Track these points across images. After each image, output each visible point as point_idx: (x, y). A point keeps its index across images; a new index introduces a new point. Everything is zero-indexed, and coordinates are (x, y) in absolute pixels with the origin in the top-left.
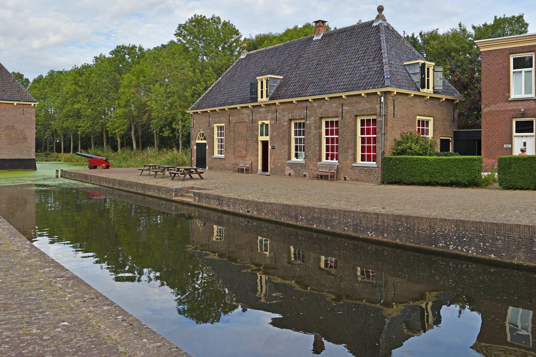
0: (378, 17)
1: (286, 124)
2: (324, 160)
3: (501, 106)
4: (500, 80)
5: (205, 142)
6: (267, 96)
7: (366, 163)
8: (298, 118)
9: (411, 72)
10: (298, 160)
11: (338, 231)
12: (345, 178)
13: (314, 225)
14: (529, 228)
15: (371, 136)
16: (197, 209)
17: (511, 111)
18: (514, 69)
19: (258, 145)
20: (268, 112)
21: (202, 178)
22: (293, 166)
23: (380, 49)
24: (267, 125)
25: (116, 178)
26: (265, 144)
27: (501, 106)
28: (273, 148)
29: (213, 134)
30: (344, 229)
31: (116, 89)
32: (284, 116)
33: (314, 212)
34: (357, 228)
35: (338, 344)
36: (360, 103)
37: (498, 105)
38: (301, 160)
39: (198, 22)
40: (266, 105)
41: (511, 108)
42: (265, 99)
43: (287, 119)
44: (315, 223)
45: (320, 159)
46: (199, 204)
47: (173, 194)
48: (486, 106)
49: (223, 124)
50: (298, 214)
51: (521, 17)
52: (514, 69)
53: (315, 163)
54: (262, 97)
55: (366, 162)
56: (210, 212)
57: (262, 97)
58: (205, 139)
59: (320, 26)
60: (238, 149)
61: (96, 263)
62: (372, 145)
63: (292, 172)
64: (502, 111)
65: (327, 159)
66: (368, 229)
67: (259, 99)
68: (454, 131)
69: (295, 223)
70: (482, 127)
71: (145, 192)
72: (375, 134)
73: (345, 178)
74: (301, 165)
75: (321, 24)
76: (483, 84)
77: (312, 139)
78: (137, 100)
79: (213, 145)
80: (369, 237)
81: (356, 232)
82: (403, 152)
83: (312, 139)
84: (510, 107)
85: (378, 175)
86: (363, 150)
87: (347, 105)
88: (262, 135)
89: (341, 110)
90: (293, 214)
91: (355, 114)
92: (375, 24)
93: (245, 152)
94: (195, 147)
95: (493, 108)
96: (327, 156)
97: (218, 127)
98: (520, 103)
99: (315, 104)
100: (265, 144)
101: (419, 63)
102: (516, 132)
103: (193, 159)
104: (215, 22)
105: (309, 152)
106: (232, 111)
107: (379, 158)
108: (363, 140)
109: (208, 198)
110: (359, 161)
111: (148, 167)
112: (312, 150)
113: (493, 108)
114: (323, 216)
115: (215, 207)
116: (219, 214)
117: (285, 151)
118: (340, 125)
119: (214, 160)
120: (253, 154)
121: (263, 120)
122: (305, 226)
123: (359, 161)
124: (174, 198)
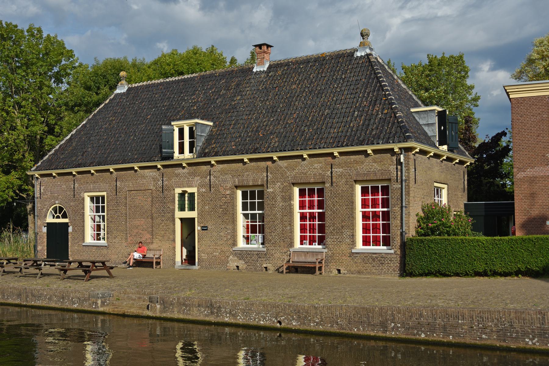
0: (362, 45)
1: (228, 192)
2: (297, 245)
4: (538, 136)
5: (66, 220)
6: (191, 151)
7: (372, 248)
8: (251, 184)
9: (421, 122)
10: (250, 246)
11: (468, 340)
12: (339, 271)
13: (420, 335)
15: (257, 212)
16: (158, 322)
18: (195, 265)
19: (174, 224)
20: (193, 174)
21: (111, 276)
22: (242, 254)
23: (382, 87)
24: (192, 195)
26: (188, 223)
28: (204, 228)
29: (83, 208)
30: (481, 338)
32: (225, 181)
33: (421, 315)
34: (505, 335)
36: (362, 163)
37: (536, 169)
38: (256, 246)
40: (189, 165)
43: (229, 185)
44: (422, 332)
45: (291, 244)
46: (164, 315)
47: (99, 302)
48: (520, 169)
49: (104, 194)
50: (387, 320)
51: (461, 57)
52: (362, 208)
53: (285, 250)
54: (181, 151)
55: (371, 247)
56: (191, 326)
57: (181, 151)
58: (65, 216)
59: (265, 52)
60: (136, 231)
62: (257, 201)
63: (241, 264)
64: (542, 177)
65: (302, 243)
66: (525, 334)
67: (176, 155)
68: (465, 204)
69: (380, 334)
70: (326, 219)
71: (27, 301)
73: (339, 271)
74: (259, 254)
75: (265, 48)
76: (516, 278)
77: (279, 215)
78: (411, 245)
79: (83, 226)
80: (528, 347)
81: (504, 341)
82: (433, 231)
83: (279, 215)
85: (396, 264)
86: (366, 229)
87: (340, 165)
88: (182, 209)
89: (329, 173)
90: (377, 321)
91: (355, 178)
92: (359, 54)
93: (148, 236)
94: (45, 230)
95: (529, 172)
96: (303, 239)
97: (92, 198)
99: (283, 164)
100: (188, 223)
101: (434, 110)
103: (39, 248)
104: (32, 35)
105: (273, 235)
106: (46, 179)
107: (397, 241)
108: (303, 217)
109: (184, 304)
110: (359, 246)
112: (279, 230)
113: (529, 172)
114: (439, 321)
115: (201, 318)
116: (302, 336)
117: (228, 234)
118: (327, 193)
119: (87, 249)
120: (166, 238)
121: (184, 187)
122: (404, 336)
123: (359, 246)
124: (101, 309)
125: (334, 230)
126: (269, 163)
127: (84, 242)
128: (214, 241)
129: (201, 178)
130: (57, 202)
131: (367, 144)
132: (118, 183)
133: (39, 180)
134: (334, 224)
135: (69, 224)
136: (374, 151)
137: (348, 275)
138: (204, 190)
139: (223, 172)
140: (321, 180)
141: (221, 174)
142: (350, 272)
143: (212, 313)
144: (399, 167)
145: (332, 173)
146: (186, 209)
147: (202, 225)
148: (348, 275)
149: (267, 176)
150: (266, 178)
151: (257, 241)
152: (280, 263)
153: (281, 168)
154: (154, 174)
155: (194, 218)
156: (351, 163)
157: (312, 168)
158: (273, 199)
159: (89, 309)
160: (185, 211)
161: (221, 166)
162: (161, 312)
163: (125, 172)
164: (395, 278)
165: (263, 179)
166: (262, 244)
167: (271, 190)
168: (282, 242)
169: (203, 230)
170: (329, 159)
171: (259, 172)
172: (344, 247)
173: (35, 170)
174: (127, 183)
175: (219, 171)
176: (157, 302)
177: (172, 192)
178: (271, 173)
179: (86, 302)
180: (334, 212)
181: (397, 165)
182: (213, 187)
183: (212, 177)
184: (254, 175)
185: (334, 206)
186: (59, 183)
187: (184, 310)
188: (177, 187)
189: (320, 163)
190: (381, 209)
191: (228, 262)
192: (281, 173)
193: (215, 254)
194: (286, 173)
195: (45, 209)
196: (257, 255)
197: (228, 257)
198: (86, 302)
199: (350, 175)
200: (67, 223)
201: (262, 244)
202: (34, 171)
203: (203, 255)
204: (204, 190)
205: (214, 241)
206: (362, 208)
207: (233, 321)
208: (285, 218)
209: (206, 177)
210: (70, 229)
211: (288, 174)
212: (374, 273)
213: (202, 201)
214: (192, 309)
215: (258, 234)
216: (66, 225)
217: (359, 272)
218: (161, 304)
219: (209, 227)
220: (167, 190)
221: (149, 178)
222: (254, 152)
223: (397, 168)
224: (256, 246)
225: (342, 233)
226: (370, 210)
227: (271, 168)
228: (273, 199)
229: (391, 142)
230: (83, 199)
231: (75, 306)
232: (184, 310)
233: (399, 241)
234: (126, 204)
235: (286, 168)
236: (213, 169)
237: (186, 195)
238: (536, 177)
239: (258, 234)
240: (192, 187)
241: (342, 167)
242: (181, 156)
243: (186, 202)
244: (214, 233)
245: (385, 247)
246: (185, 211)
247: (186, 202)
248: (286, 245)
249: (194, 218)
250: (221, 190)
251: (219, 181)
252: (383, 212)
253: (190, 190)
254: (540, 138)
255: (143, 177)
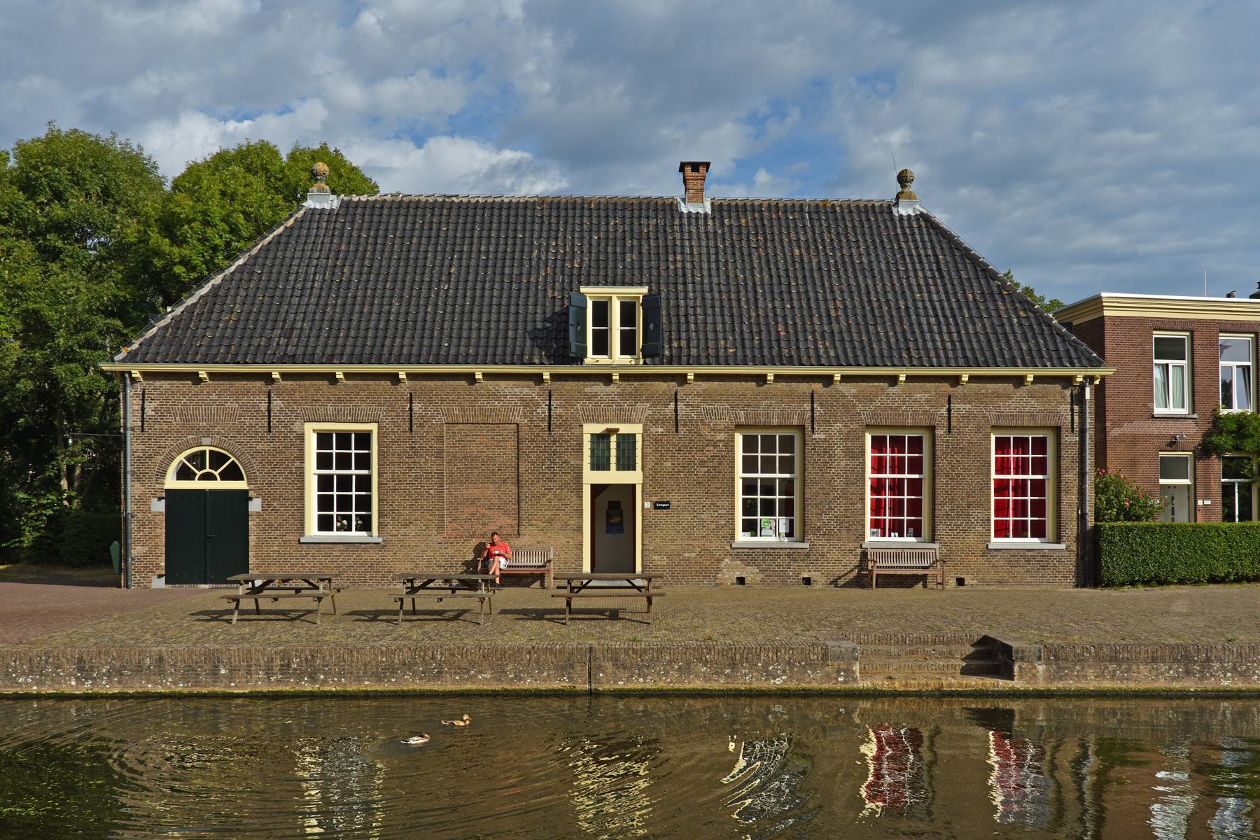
3: (1140, 427)
5: (240, 485)
14: (780, 356)
17: (1157, 436)
20: (636, 398)
25: (1092, 590)
27: (1140, 427)
31: (269, 505)
35: (181, 582)
36: (1009, 397)
39: (985, 640)
40: (624, 377)
41: (1156, 432)
42: (617, 356)
46: (1054, 686)
48: (1115, 424)
51: (619, 503)
52: (318, 468)
54: (602, 346)
55: (335, 533)
56: (1132, 704)
58: (232, 473)
61: (479, 549)
63: (750, 574)
64: (1143, 436)
72: (695, 380)
73: (960, 582)
84: (1154, 429)
85: (1070, 566)
87: (965, 399)
89: (944, 411)
91: (994, 422)
94: (160, 507)
95: (1127, 429)
98: (1171, 423)
99: (851, 389)
102: (996, 536)
107: (1071, 530)
111: (590, 584)
113: (1127, 429)
119: (314, 550)
120: (557, 525)
123: (312, 530)
125: (952, 510)
126: (817, 386)
127: (302, 534)
128: (684, 529)
129: (654, 405)
130: (206, 441)
131: (688, 364)
132: (417, 407)
133: (139, 387)
134: (952, 500)
135: (251, 494)
136: (211, 375)
137: (981, 588)
138: (660, 430)
139: (707, 397)
140: (927, 423)
141: (704, 401)
142: (982, 581)
143: (1188, 673)
144: (1076, 408)
145: (949, 410)
146: (613, 466)
147: (655, 499)
148: (981, 588)
149: (812, 410)
150: (809, 414)
151: (776, 532)
152: (838, 570)
153: (844, 396)
154: (526, 390)
155: (634, 486)
156: (986, 395)
157: (909, 399)
158: (825, 451)
159: (826, 686)
160: (609, 469)
161: (704, 385)
162: (1050, 678)
163: (440, 383)
164: (1068, 589)
165: (802, 415)
166: (787, 535)
167: (822, 436)
168: (844, 532)
169: (656, 508)
170: (945, 387)
171: (793, 401)
172: (971, 539)
173: (132, 358)
174: (440, 407)
175: (698, 395)
176: (1039, 658)
177: (576, 431)
178: (821, 404)
179: (814, 670)
180: (952, 479)
181: (1072, 404)
182: (685, 425)
183: (681, 406)
184: (779, 406)
185: (952, 468)
186: (214, 397)
187: (1114, 671)
188: (588, 421)
189: (925, 392)
190: (353, 471)
191: (719, 570)
192: (843, 405)
193: (686, 555)
194: (854, 405)
195: (159, 458)
196: (789, 555)
197: (719, 561)
198: (814, 670)
199: (984, 416)
200: (247, 491)
201: (787, 535)
202: (123, 361)
203: (656, 557)
204: (660, 430)
205: (684, 529)
206: (318, 468)
207: (1241, 685)
208: (853, 489)
209: (666, 405)
210: (255, 506)
211: (860, 407)
212: (1028, 583)
213: (657, 450)
214: (1134, 667)
215: (777, 517)
216: (244, 496)
217: (1000, 582)
218: (1048, 662)
219: (674, 503)
220: (561, 425)
221: (511, 396)
222: (293, 360)
223: (1072, 410)
224: (774, 539)
225: (968, 515)
226: (759, 475)
227: (821, 395)
228: (825, 451)
229: (537, 361)
230: (301, 437)
231: (778, 682)
232: (1114, 671)
233: (1075, 529)
234: (441, 451)
235: (855, 396)
236: (682, 391)
237: (613, 439)
238: (1135, 436)
239: (777, 517)
240: (630, 422)
241: (970, 403)
242: (603, 359)
243: (613, 452)
244: (686, 514)
245: (1036, 540)
246: (609, 469)
247: (613, 452)
248: (854, 537)
249: (634, 486)
250: (705, 431)
251: (699, 414)
252: (781, 479)
253: (625, 429)
254: (1141, 379)
255: (494, 396)
